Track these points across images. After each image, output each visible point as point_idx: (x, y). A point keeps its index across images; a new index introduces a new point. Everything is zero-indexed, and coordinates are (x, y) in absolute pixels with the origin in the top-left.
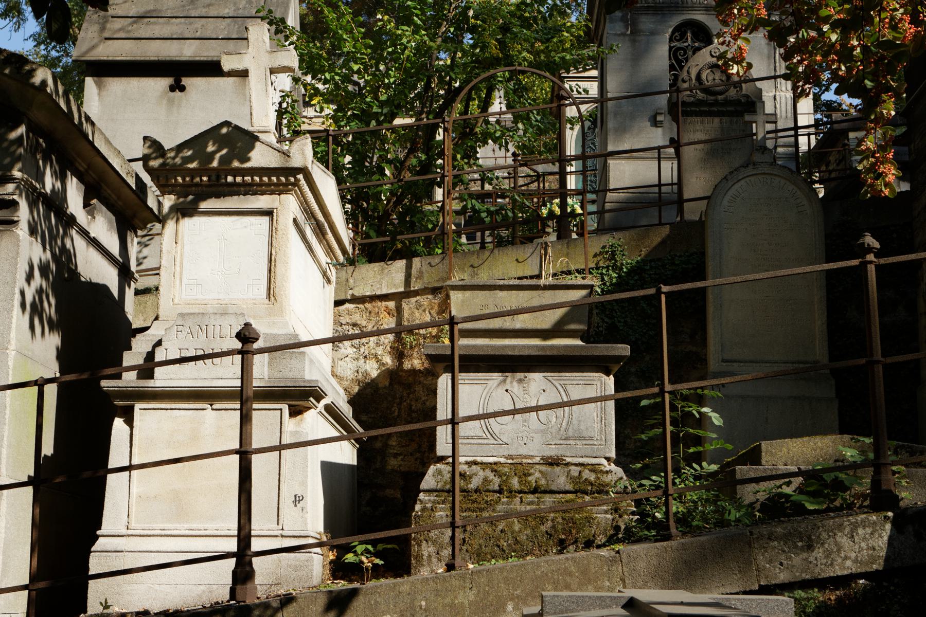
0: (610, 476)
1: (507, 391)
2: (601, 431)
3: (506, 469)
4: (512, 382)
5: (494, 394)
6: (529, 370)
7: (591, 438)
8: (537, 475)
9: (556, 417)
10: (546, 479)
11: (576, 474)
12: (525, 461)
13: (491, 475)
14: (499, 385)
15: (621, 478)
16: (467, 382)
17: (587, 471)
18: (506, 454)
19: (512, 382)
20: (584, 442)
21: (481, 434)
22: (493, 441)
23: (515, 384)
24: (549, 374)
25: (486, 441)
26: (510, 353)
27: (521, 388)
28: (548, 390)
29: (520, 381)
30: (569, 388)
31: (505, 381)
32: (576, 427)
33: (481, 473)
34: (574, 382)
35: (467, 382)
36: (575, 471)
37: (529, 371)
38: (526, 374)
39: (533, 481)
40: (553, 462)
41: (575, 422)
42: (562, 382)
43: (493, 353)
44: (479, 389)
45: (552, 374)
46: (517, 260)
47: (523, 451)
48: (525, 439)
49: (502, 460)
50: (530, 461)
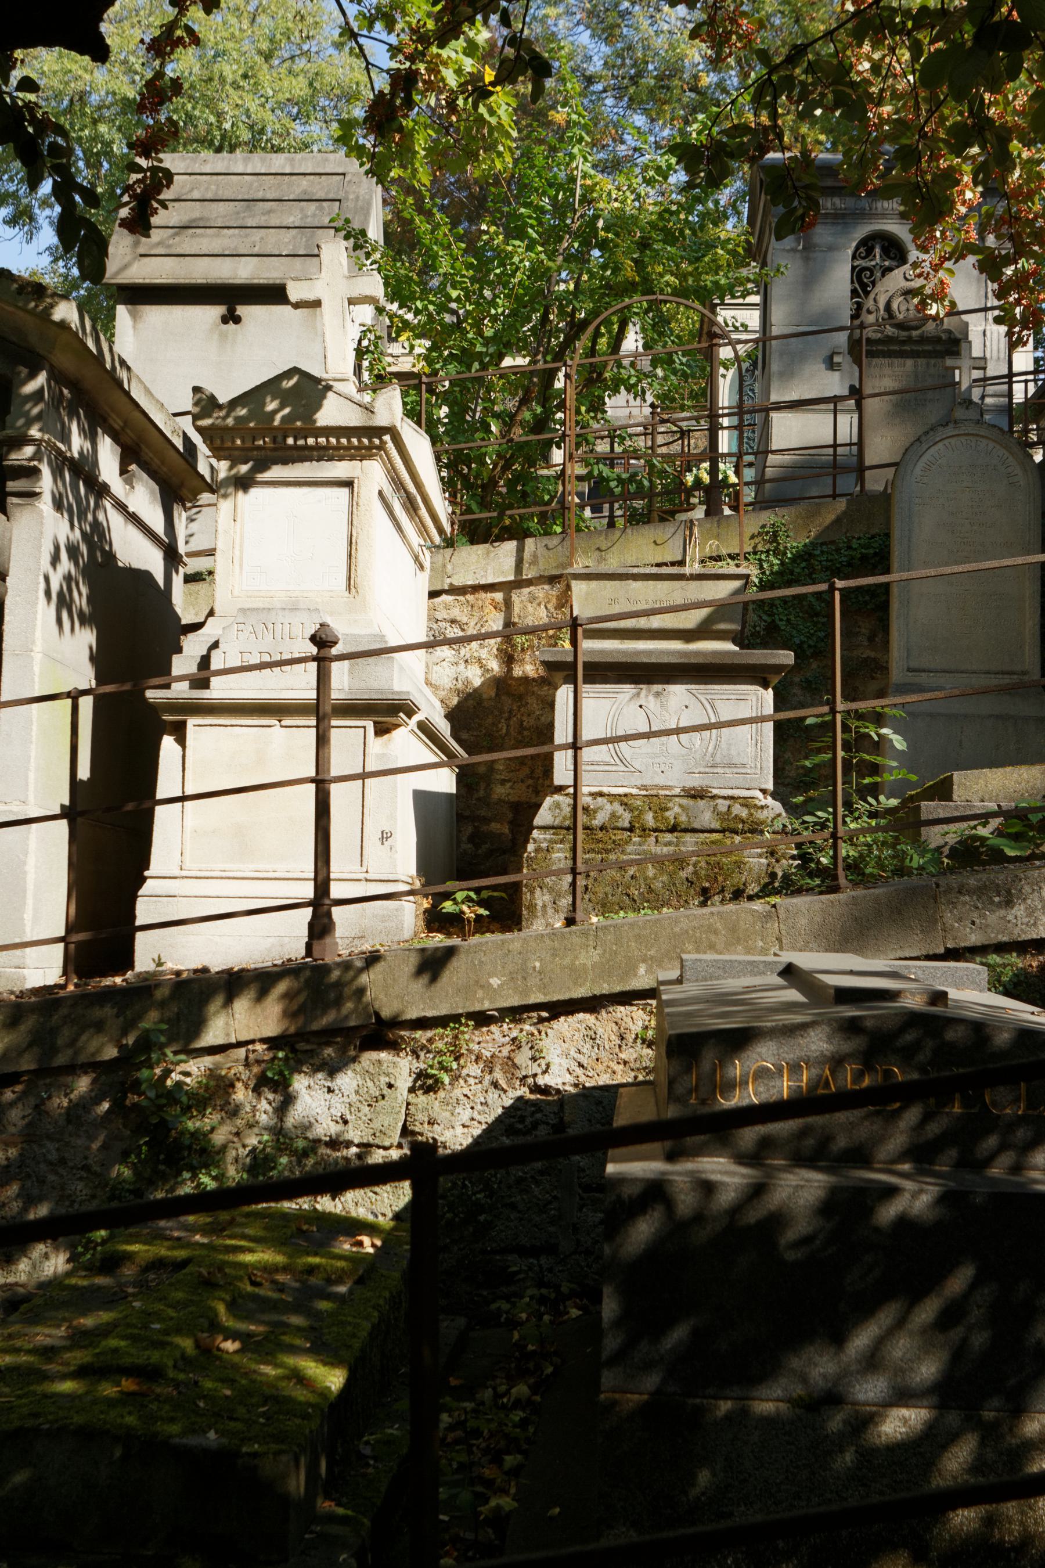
0: (765, 812)
3: (639, 803)
5: (625, 711)
7: (744, 766)
11: (724, 809)
12: (662, 792)
15: (779, 815)
17: (737, 806)
21: (608, 759)
23: (651, 698)
25: (614, 768)
26: (645, 660)
28: (691, 707)
29: (658, 695)
31: (638, 694)
33: (608, 807)
36: (722, 805)
37: (668, 682)
40: (696, 794)
41: (723, 745)
43: (624, 660)
47: (660, 780)
49: (634, 791)
50: (667, 793)
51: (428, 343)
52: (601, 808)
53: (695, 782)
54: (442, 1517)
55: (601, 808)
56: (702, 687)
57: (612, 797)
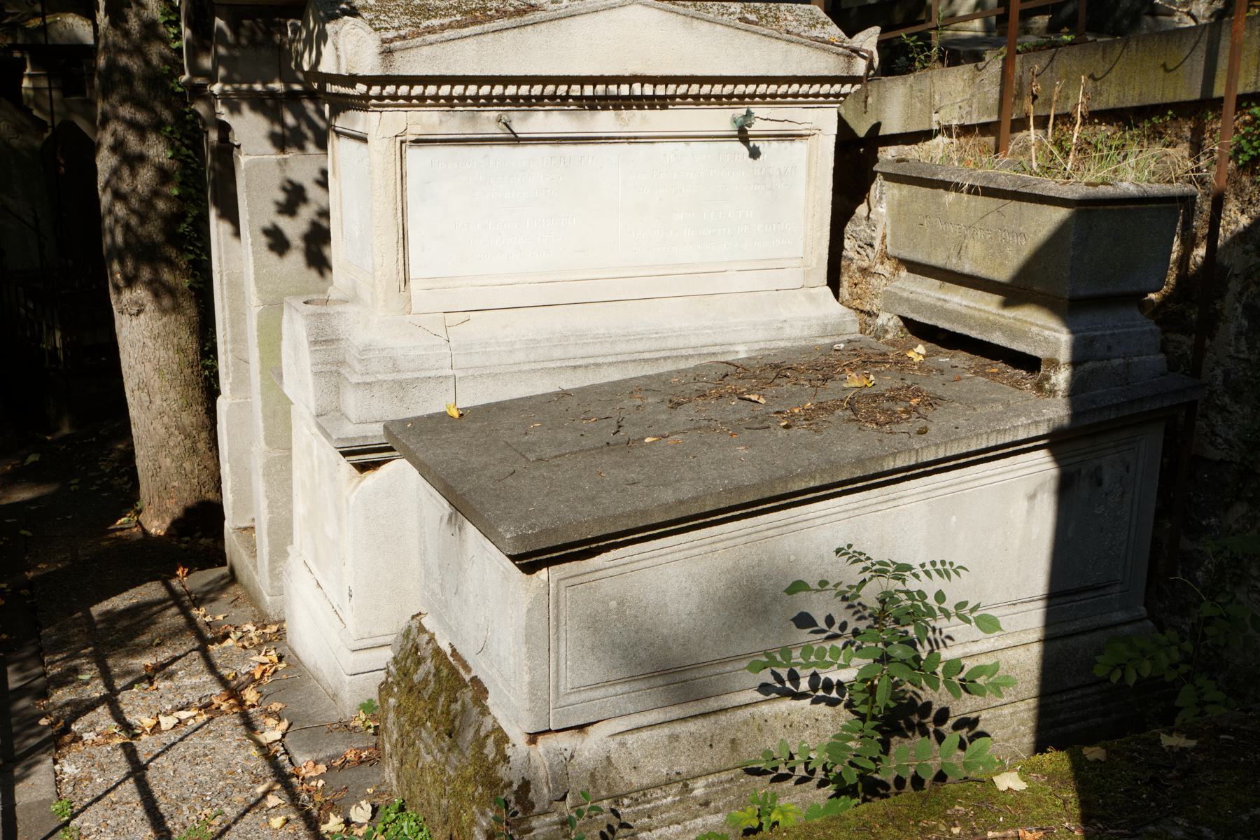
46: (1164, 66)
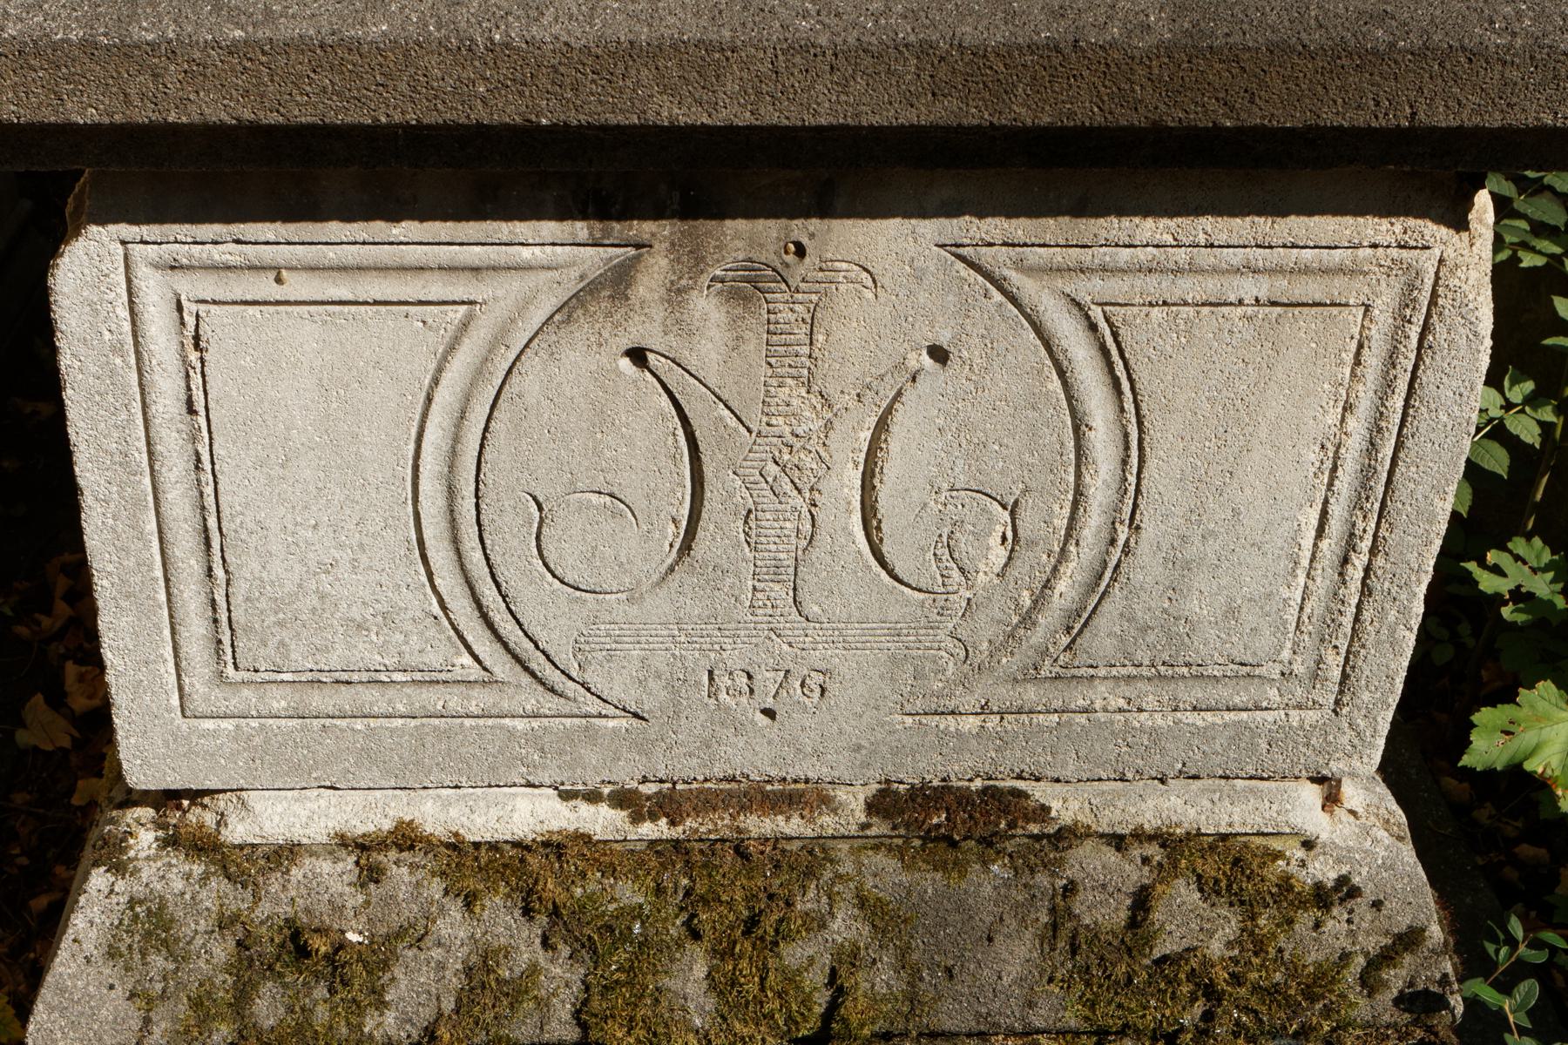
0: (1336, 923)
1: (638, 356)
2: (1331, 621)
3: (629, 893)
4: (676, 294)
5: (529, 383)
6: (825, 203)
7: (1246, 670)
8: (845, 926)
9: (1013, 541)
10: (903, 961)
11: (1109, 914)
12: (758, 825)
13: (521, 941)
14: (568, 310)
15: (1410, 939)
16: (298, 286)
17: (1185, 893)
18: (626, 774)
19: (676, 294)
20: (1197, 693)
21: (439, 653)
22: (533, 698)
23: (706, 306)
24: (995, 227)
25: (479, 699)
26: (669, 111)
27: (754, 345)
28: (969, 352)
29: (747, 288)
30: (1146, 335)
31: (618, 281)
32: (1150, 604)
33: (453, 925)
34: (1189, 287)
35: (298, 286)
36: (1102, 883)
37: (824, 209)
38: (800, 229)
39: (815, 978)
40: (953, 822)
41: (1146, 567)
42: (1088, 288)
43: (508, 111)
44: (406, 344)
45: (1019, 228)
47: (754, 755)
48: (767, 680)
49: (602, 821)
50: (793, 825)
51: (1475, 814)
52: (415, 935)
53: (959, 755)
54: (349, 518)
55: (415, 935)
56: (1053, 227)
57: (472, 866)
